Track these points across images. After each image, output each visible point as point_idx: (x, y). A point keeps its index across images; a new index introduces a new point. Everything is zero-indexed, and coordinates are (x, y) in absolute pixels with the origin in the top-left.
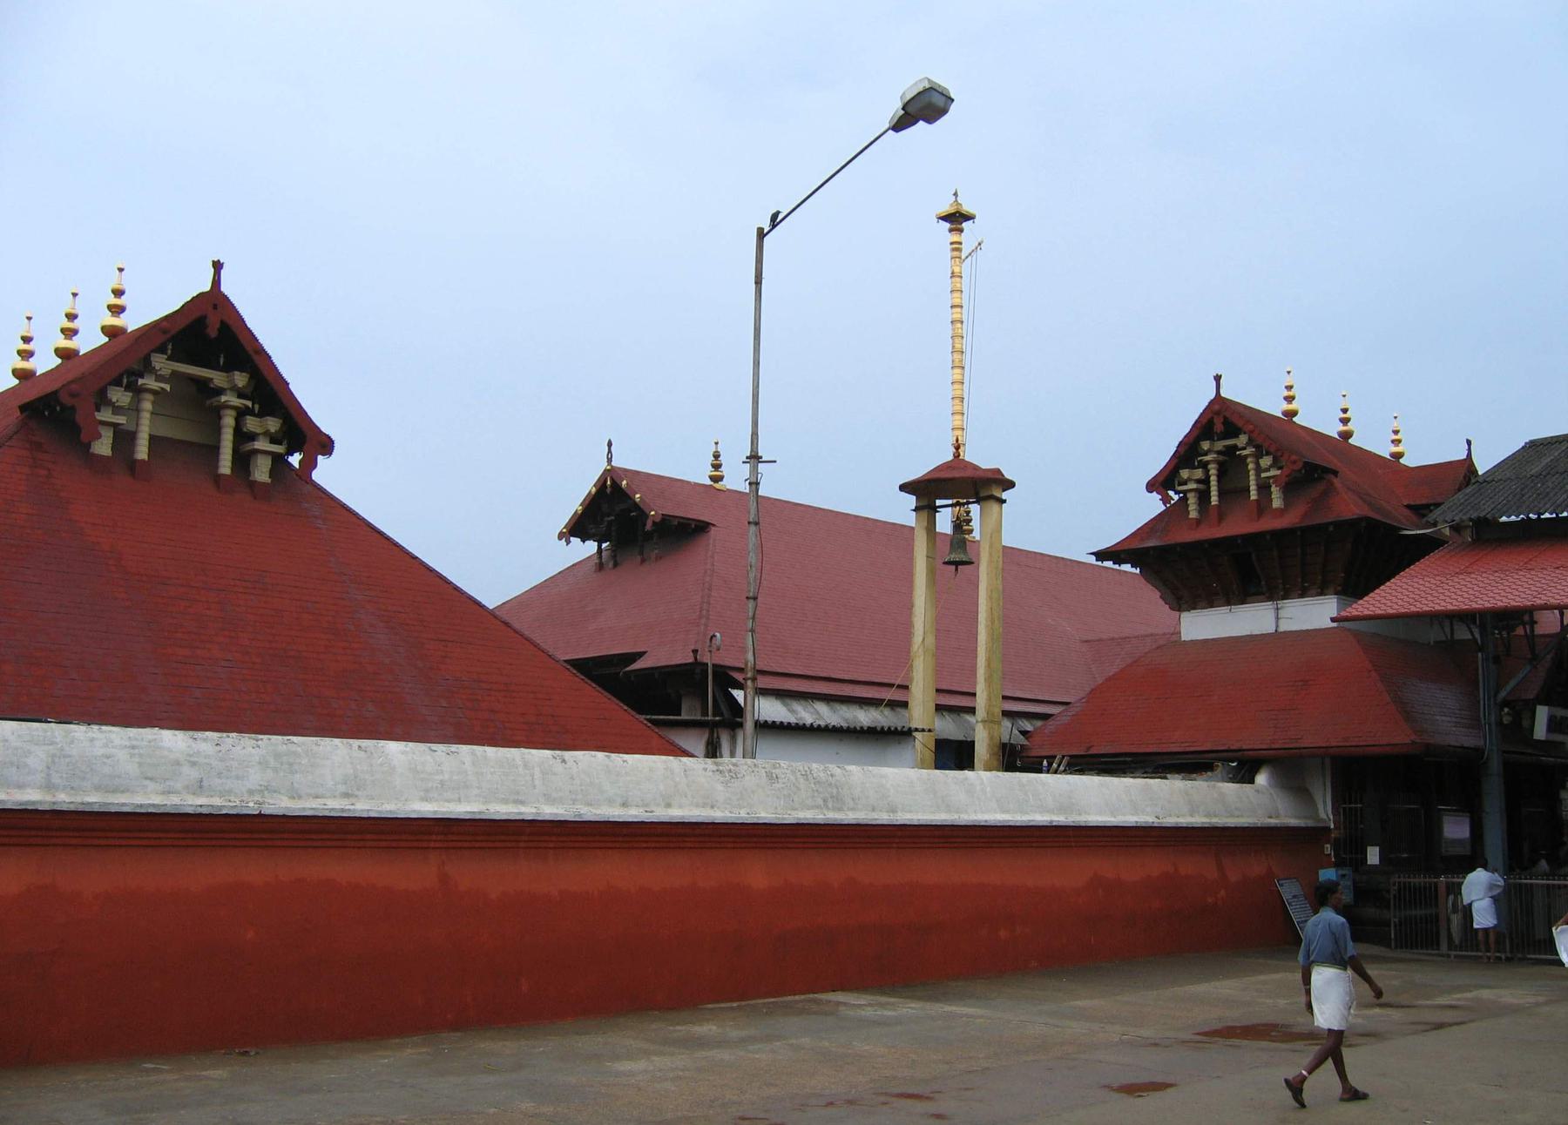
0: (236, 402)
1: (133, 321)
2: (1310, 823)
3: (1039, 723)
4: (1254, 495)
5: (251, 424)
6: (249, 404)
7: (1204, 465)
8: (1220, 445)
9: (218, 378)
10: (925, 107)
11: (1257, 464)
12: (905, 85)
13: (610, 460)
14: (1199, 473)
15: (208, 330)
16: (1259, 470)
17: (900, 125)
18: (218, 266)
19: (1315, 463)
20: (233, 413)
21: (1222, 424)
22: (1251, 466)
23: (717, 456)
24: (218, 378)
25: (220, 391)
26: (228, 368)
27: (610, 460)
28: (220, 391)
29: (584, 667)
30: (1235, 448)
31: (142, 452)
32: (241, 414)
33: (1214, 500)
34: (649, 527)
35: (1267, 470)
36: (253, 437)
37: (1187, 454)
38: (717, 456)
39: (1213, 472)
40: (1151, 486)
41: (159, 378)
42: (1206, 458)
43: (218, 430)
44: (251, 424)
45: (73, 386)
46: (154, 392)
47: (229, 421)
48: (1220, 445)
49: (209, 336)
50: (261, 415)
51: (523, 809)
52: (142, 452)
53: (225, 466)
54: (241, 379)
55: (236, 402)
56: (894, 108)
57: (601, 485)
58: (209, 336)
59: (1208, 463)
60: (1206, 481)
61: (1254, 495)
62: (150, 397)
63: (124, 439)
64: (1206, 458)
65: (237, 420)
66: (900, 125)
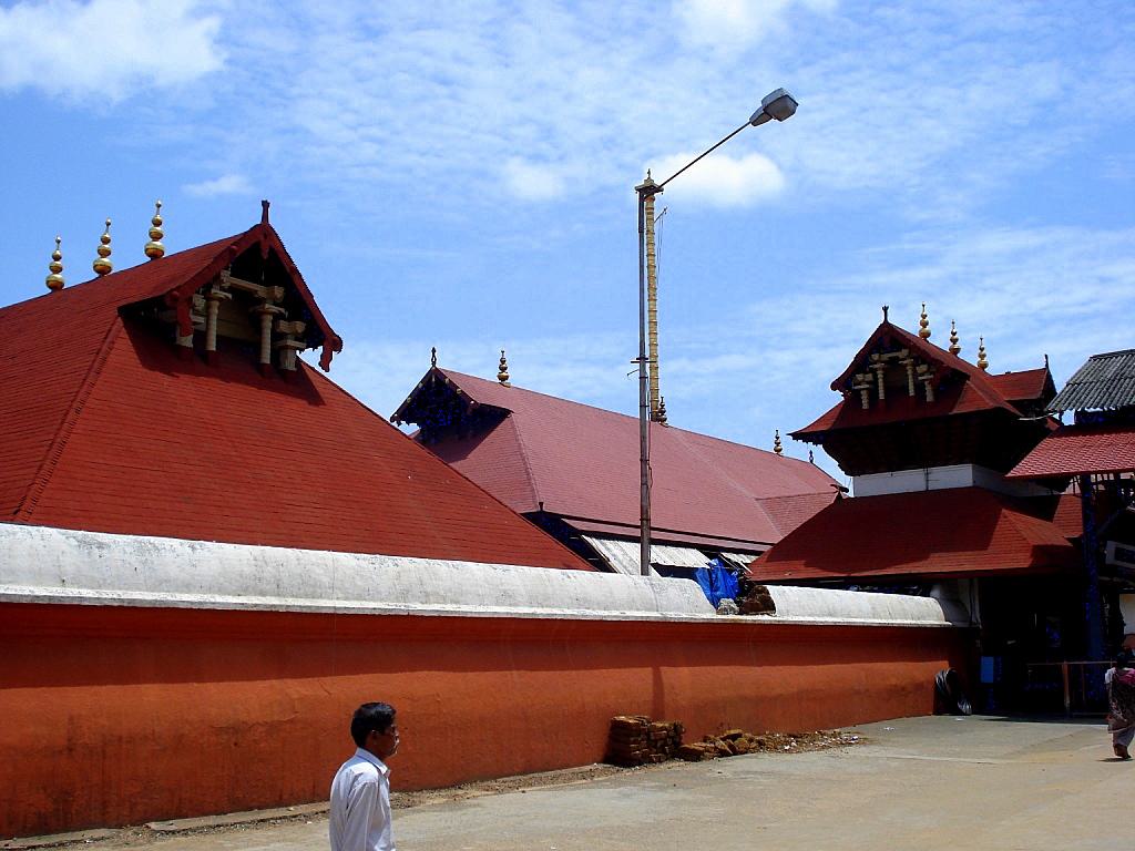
0: (275, 309)
1: (170, 246)
2: (966, 625)
3: (754, 558)
4: (912, 393)
5: (283, 326)
6: (282, 310)
7: (874, 372)
8: (886, 357)
9: (261, 290)
10: (778, 108)
11: (914, 371)
12: (768, 89)
13: (434, 363)
14: (869, 377)
15: (263, 254)
16: (915, 375)
17: (757, 120)
18: (266, 205)
19: (950, 375)
20: (270, 317)
21: (887, 338)
22: (910, 372)
23: (503, 362)
24: (261, 290)
25: (261, 301)
26: (268, 283)
27: (434, 363)
28: (261, 301)
29: (528, 516)
30: (897, 358)
31: (212, 346)
32: (277, 317)
33: (881, 396)
34: (469, 412)
35: (922, 375)
36: (283, 336)
37: (861, 362)
38: (503, 362)
39: (880, 374)
40: (834, 386)
41: (223, 289)
42: (876, 366)
43: (259, 331)
44: (283, 326)
45: (175, 292)
46: (220, 300)
47: (268, 323)
48: (886, 357)
49: (258, 260)
50: (289, 320)
51: (588, 612)
52: (212, 346)
53: (266, 359)
54: (279, 292)
55: (275, 309)
56: (756, 105)
57: (427, 380)
58: (258, 260)
59: (876, 369)
60: (874, 383)
61: (912, 393)
62: (217, 303)
63: (201, 337)
64: (876, 366)
65: (273, 322)
66: (757, 120)
